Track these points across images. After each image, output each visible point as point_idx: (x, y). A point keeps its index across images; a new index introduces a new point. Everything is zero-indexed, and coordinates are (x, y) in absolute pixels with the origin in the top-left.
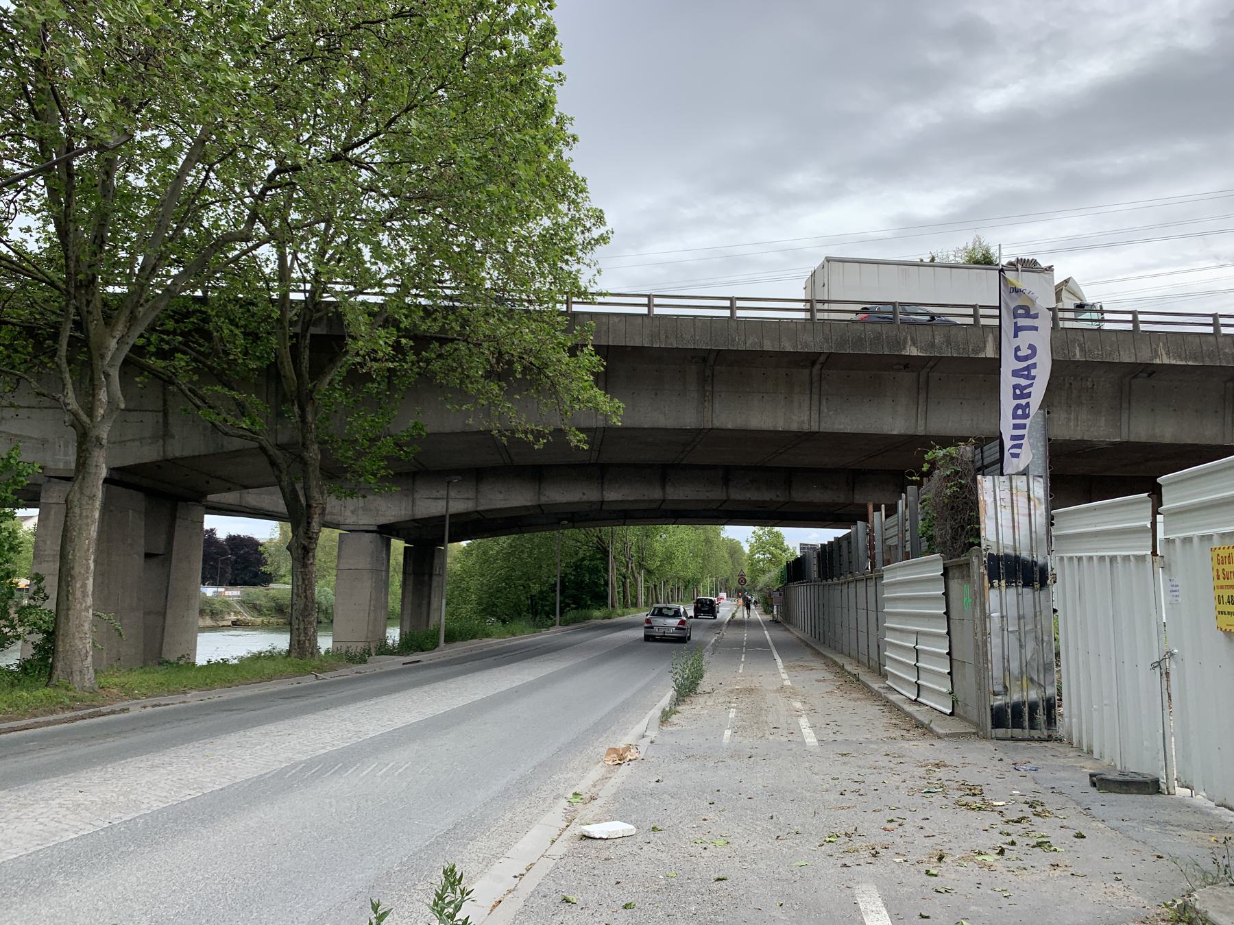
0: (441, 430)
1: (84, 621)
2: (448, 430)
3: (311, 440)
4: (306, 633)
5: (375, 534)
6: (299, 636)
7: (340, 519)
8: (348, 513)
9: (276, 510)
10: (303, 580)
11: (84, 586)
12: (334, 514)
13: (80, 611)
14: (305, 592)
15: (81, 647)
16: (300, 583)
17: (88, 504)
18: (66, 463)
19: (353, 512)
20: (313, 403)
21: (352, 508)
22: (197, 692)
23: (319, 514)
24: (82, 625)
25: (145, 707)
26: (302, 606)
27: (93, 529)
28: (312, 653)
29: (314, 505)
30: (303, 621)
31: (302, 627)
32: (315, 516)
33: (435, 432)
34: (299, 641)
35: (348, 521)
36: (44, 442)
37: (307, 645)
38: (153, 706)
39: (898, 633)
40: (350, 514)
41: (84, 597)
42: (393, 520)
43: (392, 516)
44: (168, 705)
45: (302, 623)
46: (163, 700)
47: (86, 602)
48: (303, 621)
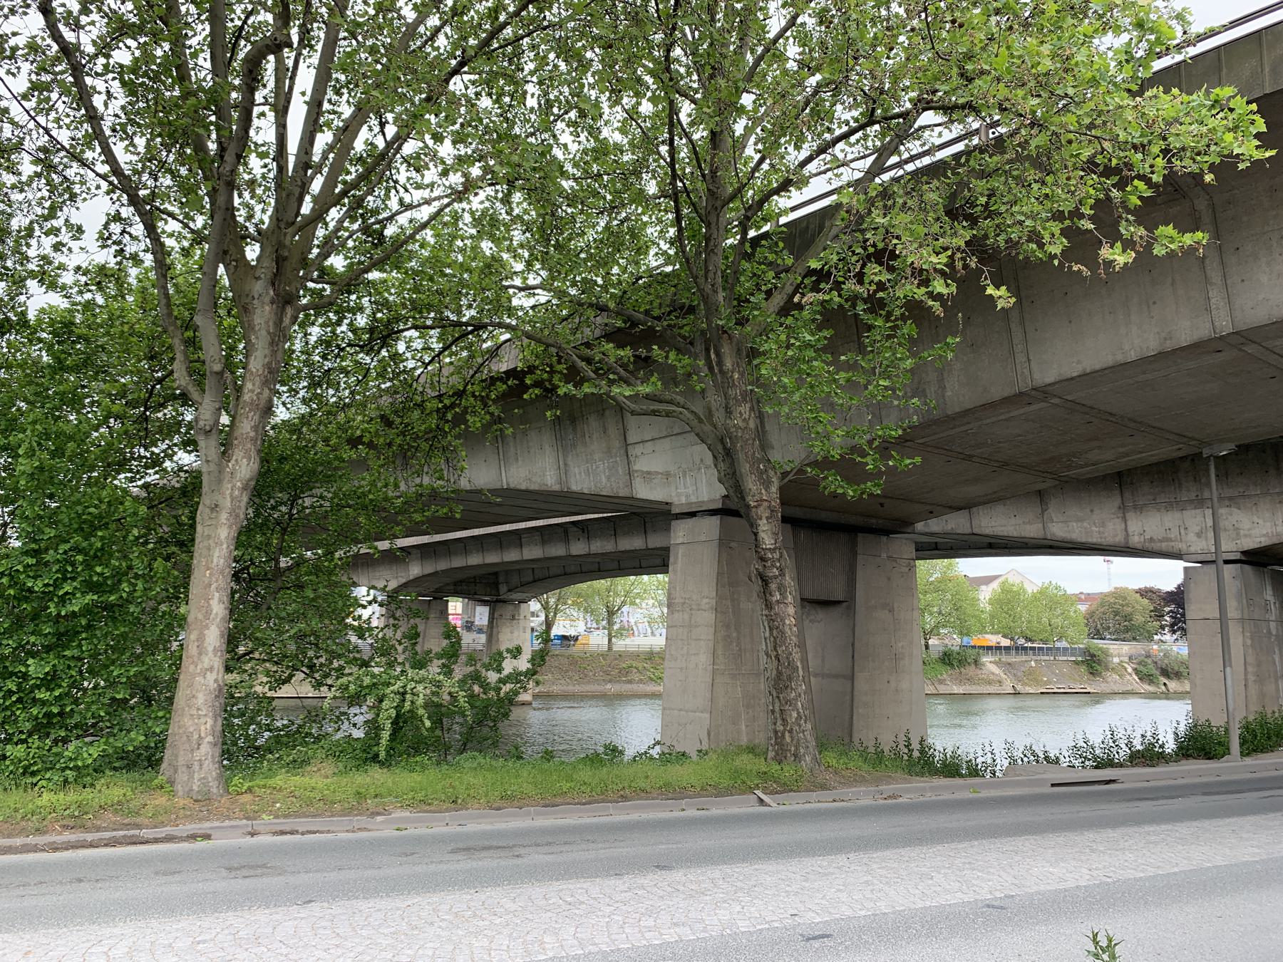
0: (1120, 358)
1: (197, 691)
2: (1132, 356)
3: (735, 398)
4: (783, 720)
5: (1239, 565)
6: (775, 724)
7: (1182, 546)
8: (1191, 537)
9: (1090, 540)
10: (771, 629)
11: (201, 638)
12: (1170, 540)
13: (193, 676)
14: (775, 649)
15: (191, 730)
16: (767, 634)
17: (210, 518)
18: (687, 496)
19: (1199, 535)
20: (730, 338)
21: (1197, 529)
22: (408, 814)
23: (767, 518)
24: (194, 696)
25: (252, 835)
26: (775, 672)
27: (217, 554)
28: (795, 755)
29: (752, 504)
30: (778, 697)
31: (777, 709)
32: (760, 522)
33: (1111, 364)
34: (776, 732)
35: (1192, 549)
36: (667, 475)
37: (788, 739)
38: (275, 833)
39: (708, 695)
40: (1195, 538)
41: (200, 654)
42: (1265, 542)
43: (1264, 535)
44: (315, 832)
45: (777, 700)
46: (302, 823)
47: (203, 662)
48: (778, 697)
